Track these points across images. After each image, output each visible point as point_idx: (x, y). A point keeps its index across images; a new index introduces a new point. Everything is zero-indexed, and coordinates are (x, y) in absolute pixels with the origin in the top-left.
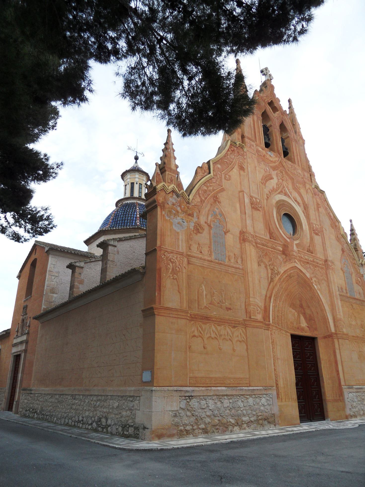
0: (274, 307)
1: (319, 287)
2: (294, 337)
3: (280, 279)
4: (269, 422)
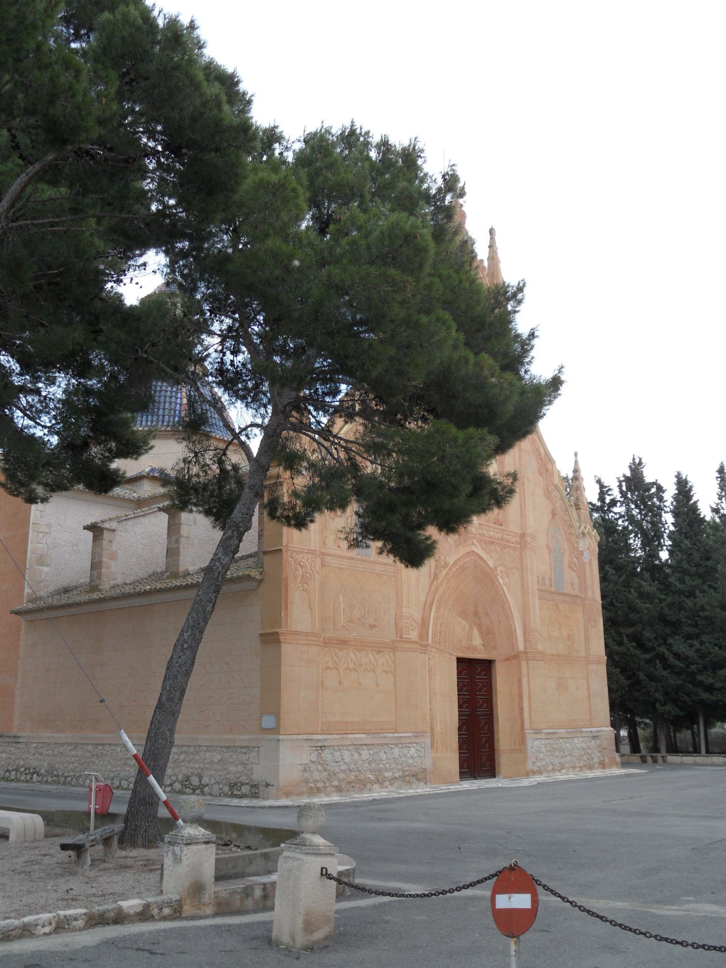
0: (436, 618)
1: (507, 580)
2: (460, 661)
3: (447, 574)
4: (418, 779)
